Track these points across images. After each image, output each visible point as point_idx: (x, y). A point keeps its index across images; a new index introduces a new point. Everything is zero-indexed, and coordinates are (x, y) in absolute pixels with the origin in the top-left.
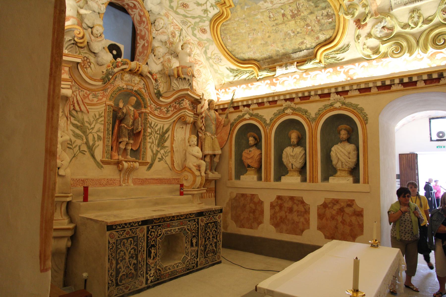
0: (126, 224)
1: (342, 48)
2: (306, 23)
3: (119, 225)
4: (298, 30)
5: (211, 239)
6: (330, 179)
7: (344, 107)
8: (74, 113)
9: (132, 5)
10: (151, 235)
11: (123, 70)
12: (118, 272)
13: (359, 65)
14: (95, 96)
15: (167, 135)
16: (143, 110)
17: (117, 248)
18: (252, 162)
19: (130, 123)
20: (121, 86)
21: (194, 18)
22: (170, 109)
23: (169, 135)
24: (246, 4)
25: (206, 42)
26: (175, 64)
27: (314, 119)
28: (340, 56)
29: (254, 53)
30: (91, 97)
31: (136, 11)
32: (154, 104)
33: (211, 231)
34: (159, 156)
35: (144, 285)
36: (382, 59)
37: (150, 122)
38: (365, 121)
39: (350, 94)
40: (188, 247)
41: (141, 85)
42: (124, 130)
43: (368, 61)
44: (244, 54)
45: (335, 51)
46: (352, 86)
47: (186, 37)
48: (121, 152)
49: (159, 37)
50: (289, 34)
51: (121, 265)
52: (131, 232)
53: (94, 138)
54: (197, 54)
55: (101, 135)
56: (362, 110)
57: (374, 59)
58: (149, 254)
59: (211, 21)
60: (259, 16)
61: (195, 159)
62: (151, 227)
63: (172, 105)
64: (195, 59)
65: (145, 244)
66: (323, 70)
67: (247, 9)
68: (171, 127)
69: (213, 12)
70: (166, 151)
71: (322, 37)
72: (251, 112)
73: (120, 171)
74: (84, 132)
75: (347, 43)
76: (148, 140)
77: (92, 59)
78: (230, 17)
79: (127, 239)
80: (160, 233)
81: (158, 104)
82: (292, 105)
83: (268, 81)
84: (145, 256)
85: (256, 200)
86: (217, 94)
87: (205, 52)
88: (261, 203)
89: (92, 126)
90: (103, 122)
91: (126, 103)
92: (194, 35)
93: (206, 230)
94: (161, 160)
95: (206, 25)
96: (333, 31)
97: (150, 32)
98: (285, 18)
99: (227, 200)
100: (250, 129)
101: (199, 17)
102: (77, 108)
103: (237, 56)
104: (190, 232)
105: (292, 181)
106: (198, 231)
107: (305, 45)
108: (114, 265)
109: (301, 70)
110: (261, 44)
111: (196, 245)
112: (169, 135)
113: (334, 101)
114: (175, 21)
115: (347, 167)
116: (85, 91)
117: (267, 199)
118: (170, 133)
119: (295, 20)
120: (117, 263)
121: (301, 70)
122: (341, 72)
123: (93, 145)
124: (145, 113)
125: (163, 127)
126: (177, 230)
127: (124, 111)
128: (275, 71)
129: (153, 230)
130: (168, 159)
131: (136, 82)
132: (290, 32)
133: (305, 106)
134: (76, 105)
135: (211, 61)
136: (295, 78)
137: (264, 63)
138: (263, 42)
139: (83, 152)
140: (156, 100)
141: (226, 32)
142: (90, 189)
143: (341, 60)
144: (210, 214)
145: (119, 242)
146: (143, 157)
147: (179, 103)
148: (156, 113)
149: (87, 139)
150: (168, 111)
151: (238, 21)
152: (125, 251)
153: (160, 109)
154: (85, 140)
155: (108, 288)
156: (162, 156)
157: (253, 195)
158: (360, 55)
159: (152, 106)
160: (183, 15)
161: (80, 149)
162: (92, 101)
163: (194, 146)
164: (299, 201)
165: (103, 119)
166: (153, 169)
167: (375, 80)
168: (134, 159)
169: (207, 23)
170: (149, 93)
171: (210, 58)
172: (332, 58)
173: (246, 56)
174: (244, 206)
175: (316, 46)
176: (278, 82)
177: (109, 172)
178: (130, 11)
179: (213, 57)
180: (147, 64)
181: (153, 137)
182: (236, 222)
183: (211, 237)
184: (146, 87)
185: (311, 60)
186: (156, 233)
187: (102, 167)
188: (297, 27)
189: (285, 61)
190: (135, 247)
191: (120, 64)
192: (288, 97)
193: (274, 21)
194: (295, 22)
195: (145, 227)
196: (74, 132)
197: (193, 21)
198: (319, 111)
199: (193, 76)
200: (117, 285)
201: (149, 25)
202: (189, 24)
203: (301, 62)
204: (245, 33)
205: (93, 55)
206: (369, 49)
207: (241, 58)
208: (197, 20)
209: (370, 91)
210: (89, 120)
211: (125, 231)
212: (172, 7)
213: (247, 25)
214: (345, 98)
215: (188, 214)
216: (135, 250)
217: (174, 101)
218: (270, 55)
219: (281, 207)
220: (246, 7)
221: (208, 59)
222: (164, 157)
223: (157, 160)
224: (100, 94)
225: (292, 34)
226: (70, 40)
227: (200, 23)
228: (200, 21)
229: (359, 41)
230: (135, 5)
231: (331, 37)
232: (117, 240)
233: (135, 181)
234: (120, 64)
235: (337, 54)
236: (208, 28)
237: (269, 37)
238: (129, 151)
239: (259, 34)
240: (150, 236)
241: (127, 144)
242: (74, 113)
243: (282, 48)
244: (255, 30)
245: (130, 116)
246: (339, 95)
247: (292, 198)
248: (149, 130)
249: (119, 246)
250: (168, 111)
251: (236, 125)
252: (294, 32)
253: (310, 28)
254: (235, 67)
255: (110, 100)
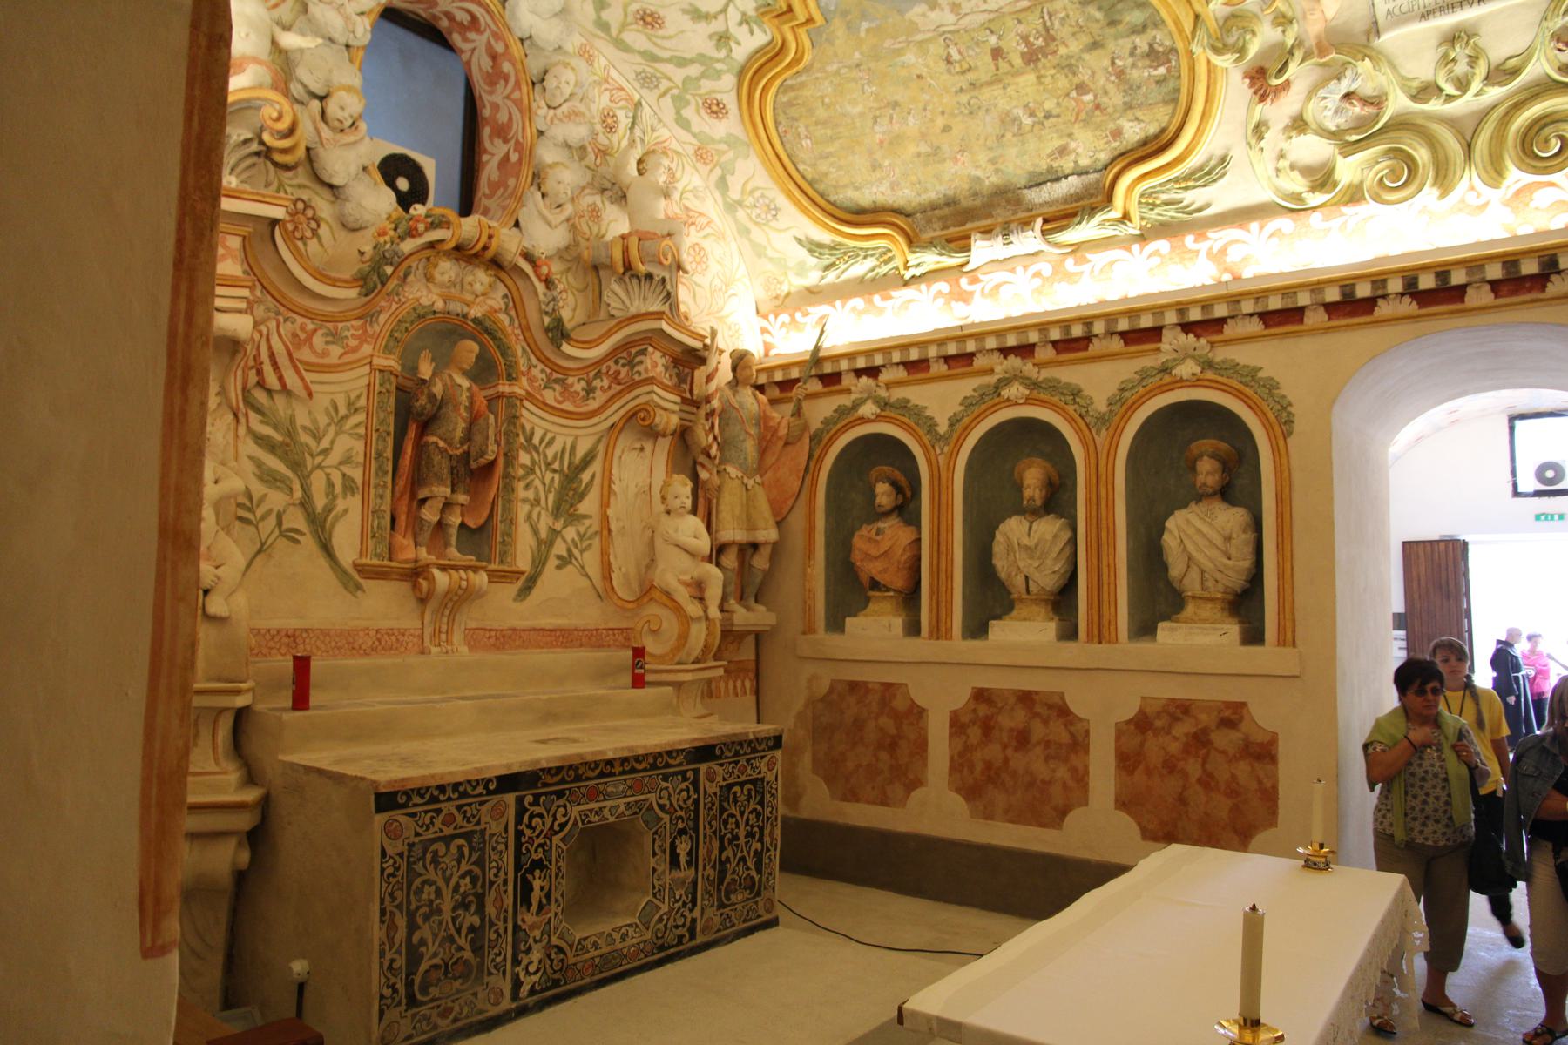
0: (442, 788)
1: (1201, 168)
2: (1076, 81)
3: (419, 792)
4: (1049, 105)
5: (742, 840)
6: (1159, 631)
7: (1209, 375)
8: (260, 396)
9: (463, 17)
10: (529, 826)
11: (432, 245)
12: (414, 957)
13: (1262, 228)
14: (335, 337)
15: (585, 477)
16: (504, 388)
17: (412, 874)
18: (885, 570)
19: (459, 434)
20: (425, 302)
21: (682, 62)
22: (597, 383)
23: (593, 477)
24: (864, 16)
25: (723, 147)
26: (616, 224)
27: (1103, 420)
28: (1195, 197)
29: (894, 186)
30: (318, 340)
31: (480, 40)
32: (541, 366)
33: (742, 813)
34: (560, 548)
35: (506, 1004)
36: (1344, 209)
37: (528, 428)
38: (1283, 424)
39: (1229, 330)
40: (660, 870)
41: (497, 300)
42: (437, 458)
43: (1294, 215)
44: (857, 189)
45: (1176, 180)
46: (1238, 302)
47: (653, 130)
48: (426, 535)
49: (560, 131)
50: (1016, 119)
51: (425, 932)
52: (459, 818)
53: (331, 485)
54: (694, 191)
55: (357, 474)
56: (1271, 386)
57: (1314, 209)
58: (524, 894)
59: (741, 74)
60: (910, 57)
61: (685, 561)
62: (530, 799)
63: (604, 369)
64: (687, 209)
65: (509, 860)
66: (1136, 247)
67: (868, 31)
68: (601, 448)
69: (750, 41)
70: (582, 530)
71: (1133, 132)
72: (883, 393)
73: (423, 601)
74: (296, 466)
75: (1219, 153)
76: (522, 493)
77: (323, 206)
78: (807, 59)
79: (447, 840)
80: (561, 820)
81: (555, 367)
82: (1028, 368)
83: (943, 286)
84: (509, 901)
85: (899, 704)
86: (764, 331)
87: (722, 184)
88: (917, 713)
89: (325, 444)
90: (362, 431)
91: (443, 362)
92: (684, 124)
93: (723, 810)
94: (564, 561)
95: (725, 87)
96: (1169, 109)
97: (527, 112)
98: (1002, 64)
99: (799, 705)
100: (881, 452)
101: (701, 59)
102: (271, 379)
103: (832, 198)
104: (666, 818)
105: (1025, 635)
106: (696, 811)
107: (1072, 157)
108: (401, 933)
109: (1057, 245)
110: (919, 155)
111: (689, 863)
112: (593, 477)
113: (1175, 355)
114: (614, 73)
115: (1220, 587)
116: (300, 320)
117: (940, 699)
118: (596, 467)
119: (1036, 69)
120: (412, 927)
121: (1057, 245)
122: (1198, 252)
123: (329, 509)
124: (511, 396)
125: (573, 448)
126: (622, 808)
127: (438, 389)
128: (967, 249)
129: (537, 810)
130: (591, 560)
131: (478, 288)
132: (1019, 112)
133: (1071, 374)
134: (267, 368)
135: (741, 214)
136: (1037, 274)
137: (929, 221)
138: (924, 148)
139: (291, 536)
140: (549, 352)
141: (793, 112)
142: (316, 665)
143: (1199, 210)
144: (737, 754)
145: (418, 850)
146: (503, 554)
147: (631, 364)
148: (549, 396)
149: (306, 489)
150: (590, 390)
151: (837, 73)
152: (441, 883)
153: (562, 382)
154: (298, 494)
155: (381, 1013)
156: (569, 551)
157: (888, 686)
158: (1264, 195)
159: (535, 372)
160: (643, 54)
161: (280, 524)
162: (325, 354)
163: (681, 515)
164: (1050, 707)
165: (361, 417)
166: (537, 594)
167: (1319, 282)
168: (471, 559)
169: (729, 81)
170: (525, 329)
171: (740, 203)
172: (1167, 203)
173: (866, 196)
174: (858, 724)
175: (1112, 161)
176: (976, 287)
177: (384, 605)
178: (456, 39)
179: (749, 201)
180: (517, 224)
181: (537, 482)
182: (830, 780)
183: (742, 834)
184: (515, 305)
185: (1093, 211)
186: (549, 821)
187: (359, 587)
188: (1045, 95)
189: (1001, 215)
190: (476, 870)
191: (421, 227)
192: (1011, 341)
193: (963, 73)
194: (1039, 77)
195: (510, 798)
196: (259, 464)
197: (679, 74)
198: (1122, 390)
199: (679, 267)
200: (412, 1001)
201: (524, 88)
202: (664, 84)
203: (1059, 218)
204: (862, 115)
205: (326, 192)
206: (1296, 174)
207: (847, 204)
208: (694, 70)
209: (1301, 321)
210: (314, 421)
211: (439, 811)
212: (604, 26)
213: (868, 89)
214: (1212, 344)
215: (660, 754)
216: (474, 881)
217: (613, 354)
218: (951, 193)
219: (988, 727)
220: (865, 25)
221: (732, 207)
222: (576, 552)
223: (552, 562)
224: (351, 329)
225: (1027, 121)
226: (246, 141)
227: (704, 82)
228: (703, 75)
229: (1262, 144)
230: (474, 18)
231: (1163, 130)
232: (411, 845)
233: (476, 639)
234: (421, 227)
235: (1186, 188)
236: (730, 100)
237: (946, 129)
238: (454, 532)
239: (910, 119)
240: (528, 832)
241: (447, 505)
242: (260, 396)
243: (991, 168)
244: (896, 104)
245: (456, 406)
246: (1191, 336)
247: (1026, 698)
248: (524, 458)
249: (419, 867)
250: (590, 390)
251: (831, 441)
252: (1032, 114)
253: (1089, 97)
254: (825, 237)
255: (388, 350)
